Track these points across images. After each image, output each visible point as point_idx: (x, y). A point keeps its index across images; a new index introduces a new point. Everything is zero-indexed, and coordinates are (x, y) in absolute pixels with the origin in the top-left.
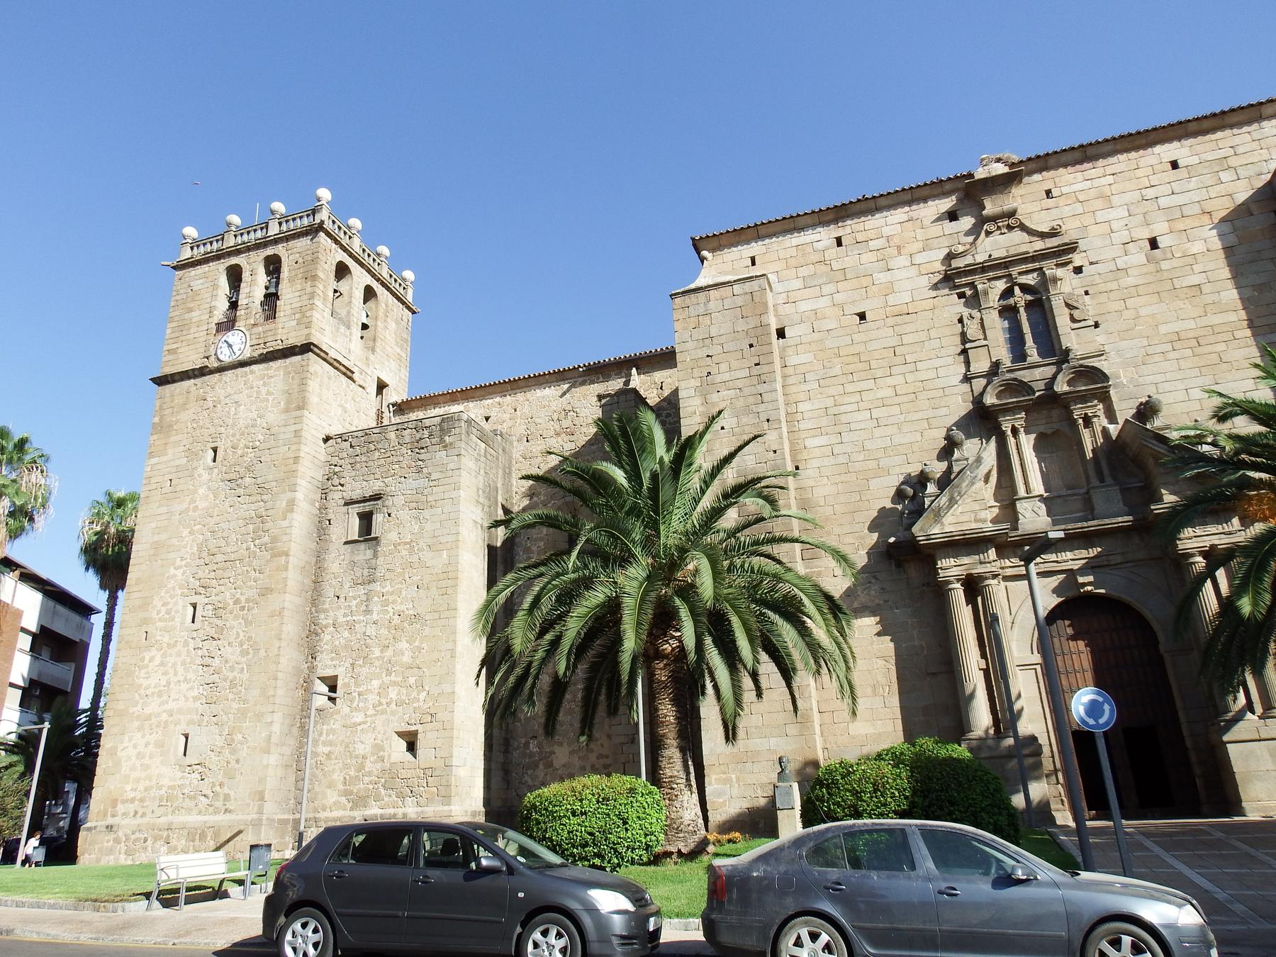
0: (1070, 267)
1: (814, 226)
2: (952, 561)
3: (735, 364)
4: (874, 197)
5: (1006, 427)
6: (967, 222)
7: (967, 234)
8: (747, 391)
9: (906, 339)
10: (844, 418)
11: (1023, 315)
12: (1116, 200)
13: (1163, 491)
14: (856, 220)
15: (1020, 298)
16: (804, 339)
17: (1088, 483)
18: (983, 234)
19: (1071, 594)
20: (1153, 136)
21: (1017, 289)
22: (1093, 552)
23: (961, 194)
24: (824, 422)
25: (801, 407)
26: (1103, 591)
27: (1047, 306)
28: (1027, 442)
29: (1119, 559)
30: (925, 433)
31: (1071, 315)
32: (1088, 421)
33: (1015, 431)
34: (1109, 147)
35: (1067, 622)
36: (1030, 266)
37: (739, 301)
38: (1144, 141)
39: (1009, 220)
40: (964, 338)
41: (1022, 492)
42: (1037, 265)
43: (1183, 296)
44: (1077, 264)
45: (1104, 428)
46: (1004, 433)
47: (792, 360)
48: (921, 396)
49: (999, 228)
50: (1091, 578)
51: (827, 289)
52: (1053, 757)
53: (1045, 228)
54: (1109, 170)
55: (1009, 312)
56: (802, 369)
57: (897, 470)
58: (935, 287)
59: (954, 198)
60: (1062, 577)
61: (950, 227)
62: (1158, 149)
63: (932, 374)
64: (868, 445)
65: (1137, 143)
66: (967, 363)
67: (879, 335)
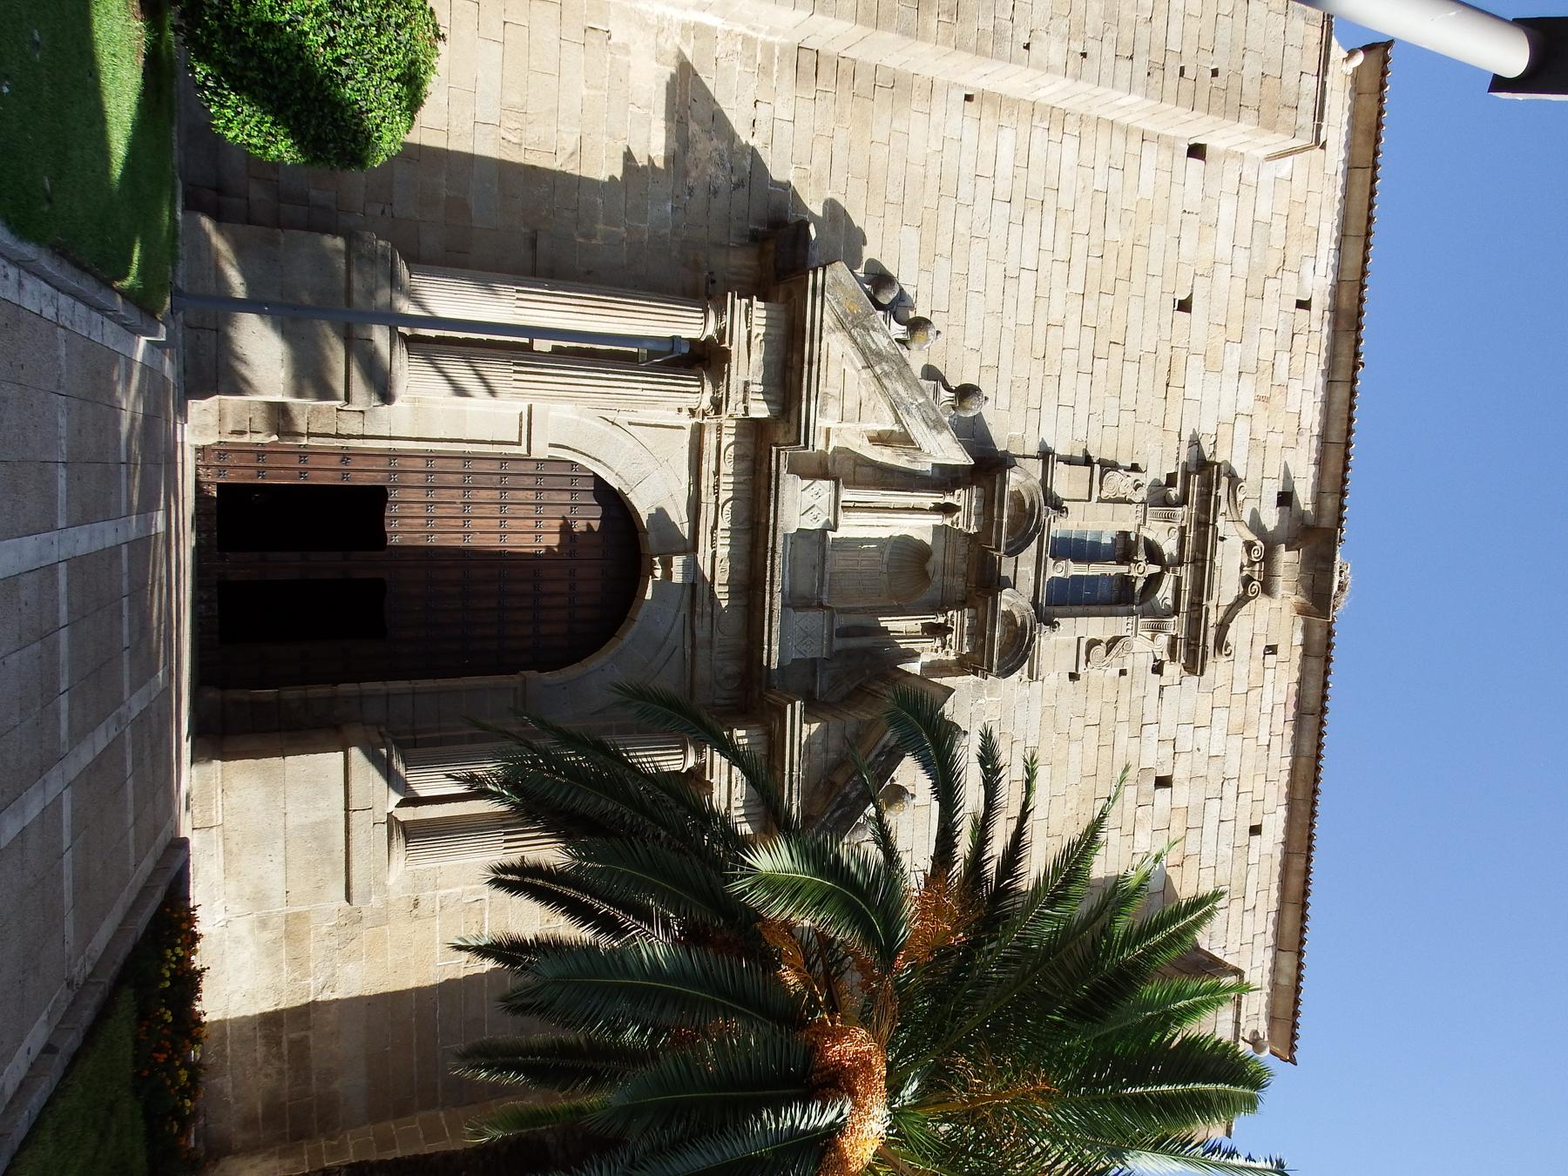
0: (1166, 657)
1: (1339, 269)
2: (759, 330)
3: (1193, 27)
4: (1354, 381)
5: (958, 498)
6: (1271, 518)
7: (1255, 515)
8: (1143, 31)
9: (1130, 368)
10: (1033, 217)
11: (1112, 569)
12: (1236, 741)
13: (815, 726)
14: (1325, 342)
15: (1142, 570)
16: (1176, 190)
17: (843, 611)
18: (1251, 537)
19: (652, 539)
20: (1303, 808)
21: (1155, 569)
22: (722, 593)
23: (1310, 521)
24: (1036, 179)
25: (1071, 144)
26: (648, 596)
27: (1121, 609)
28: (920, 528)
29: (702, 633)
30: (976, 356)
31: (1099, 642)
32: (934, 631)
33: (948, 509)
34: (1307, 746)
35: (596, 525)
36: (1185, 598)
37: (1290, 79)
38: (1299, 796)
39: (1259, 581)
40: (1109, 466)
41: (847, 495)
42: (1184, 607)
43: (1082, 810)
44: (1167, 668)
45: (918, 655)
46: (951, 491)
47: (1150, 153)
48: (1037, 367)
49: (1253, 564)
50: (677, 578)
51: (1241, 257)
52: (338, 436)
53: (1231, 636)
54: (1276, 741)
55: (1124, 548)
56: (1132, 167)
57: (924, 289)
58: (1195, 442)
59: (1309, 508)
60: (685, 531)
61: (1273, 489)
62: (1282, 812)
63: (1066, 398)
64: (979, 248)
65: (1300, 786)
66: (1069, 461)
67: (1150, 325)
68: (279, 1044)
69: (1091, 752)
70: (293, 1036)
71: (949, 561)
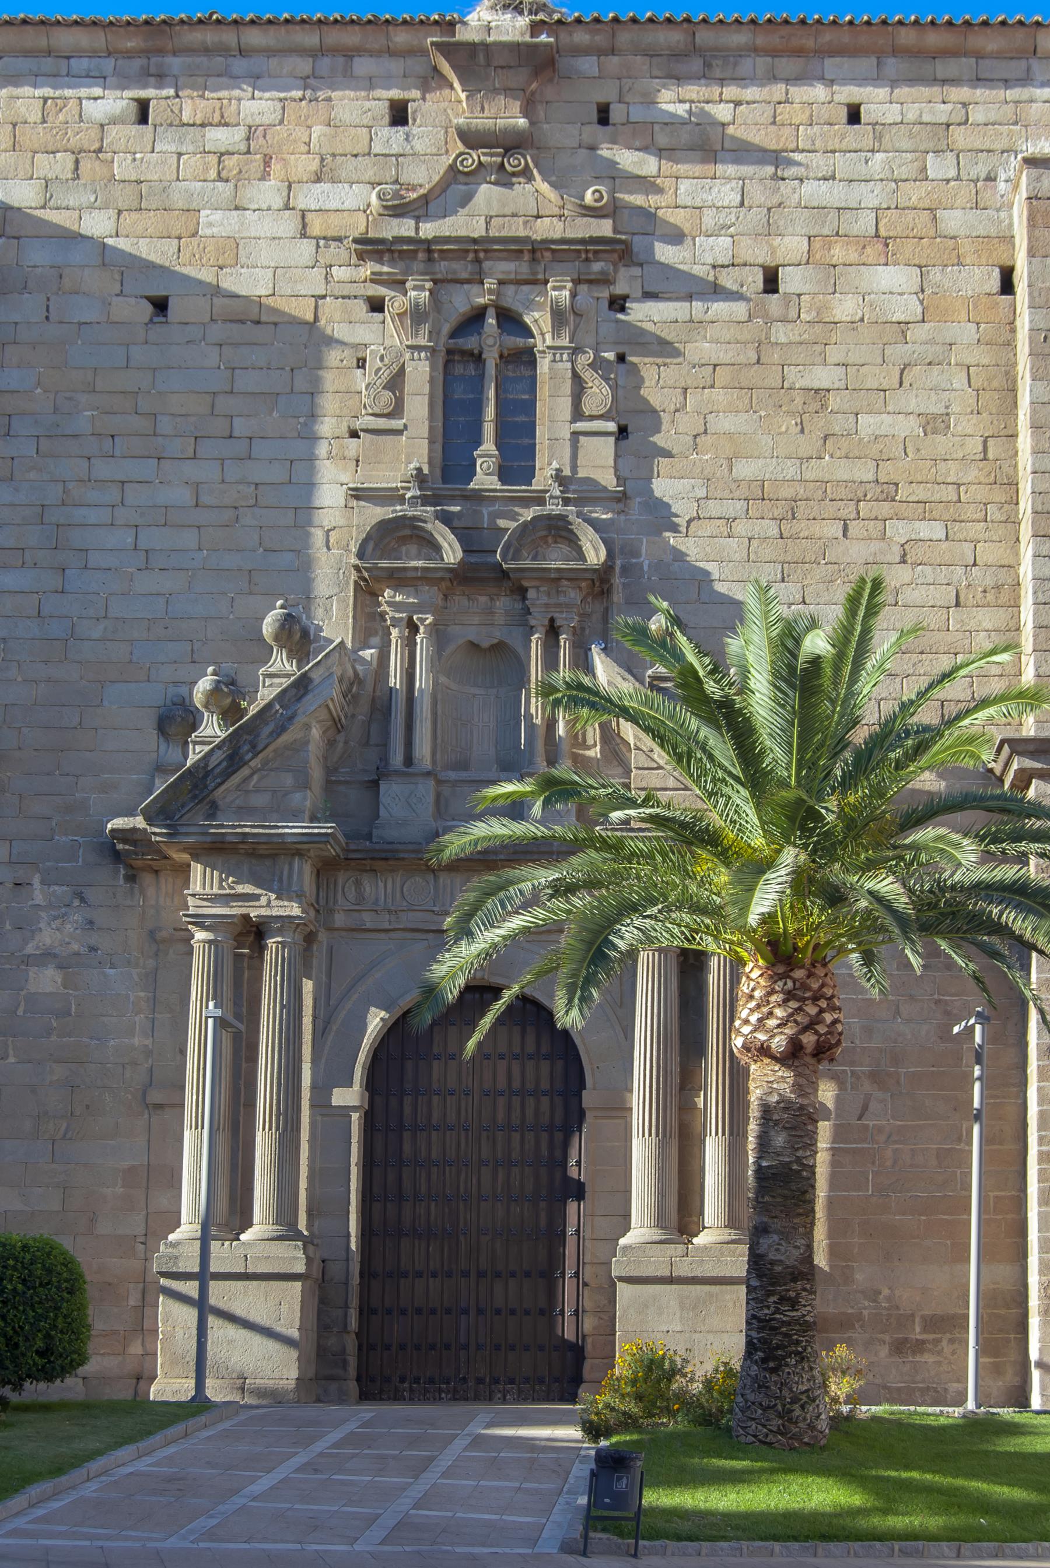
44: (619, 289)
68: (923, 1342)
69: (718, 395)
70: (918, 1329)
71: (476, 620)
